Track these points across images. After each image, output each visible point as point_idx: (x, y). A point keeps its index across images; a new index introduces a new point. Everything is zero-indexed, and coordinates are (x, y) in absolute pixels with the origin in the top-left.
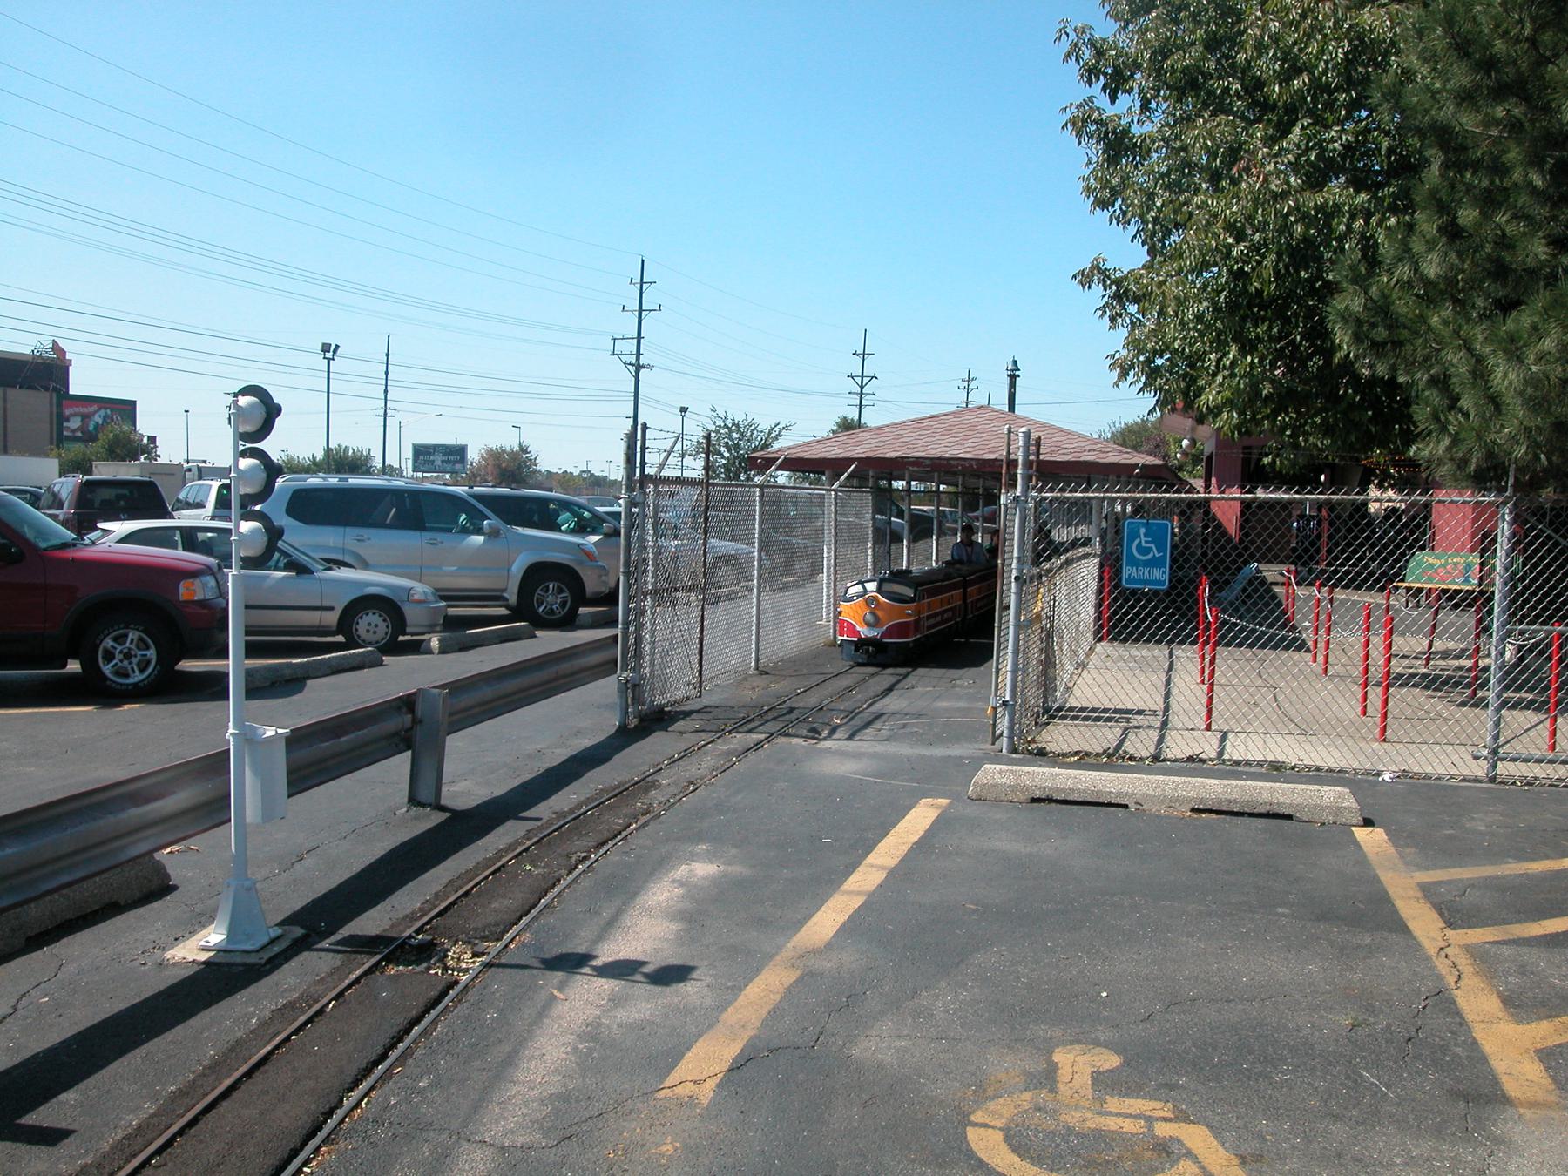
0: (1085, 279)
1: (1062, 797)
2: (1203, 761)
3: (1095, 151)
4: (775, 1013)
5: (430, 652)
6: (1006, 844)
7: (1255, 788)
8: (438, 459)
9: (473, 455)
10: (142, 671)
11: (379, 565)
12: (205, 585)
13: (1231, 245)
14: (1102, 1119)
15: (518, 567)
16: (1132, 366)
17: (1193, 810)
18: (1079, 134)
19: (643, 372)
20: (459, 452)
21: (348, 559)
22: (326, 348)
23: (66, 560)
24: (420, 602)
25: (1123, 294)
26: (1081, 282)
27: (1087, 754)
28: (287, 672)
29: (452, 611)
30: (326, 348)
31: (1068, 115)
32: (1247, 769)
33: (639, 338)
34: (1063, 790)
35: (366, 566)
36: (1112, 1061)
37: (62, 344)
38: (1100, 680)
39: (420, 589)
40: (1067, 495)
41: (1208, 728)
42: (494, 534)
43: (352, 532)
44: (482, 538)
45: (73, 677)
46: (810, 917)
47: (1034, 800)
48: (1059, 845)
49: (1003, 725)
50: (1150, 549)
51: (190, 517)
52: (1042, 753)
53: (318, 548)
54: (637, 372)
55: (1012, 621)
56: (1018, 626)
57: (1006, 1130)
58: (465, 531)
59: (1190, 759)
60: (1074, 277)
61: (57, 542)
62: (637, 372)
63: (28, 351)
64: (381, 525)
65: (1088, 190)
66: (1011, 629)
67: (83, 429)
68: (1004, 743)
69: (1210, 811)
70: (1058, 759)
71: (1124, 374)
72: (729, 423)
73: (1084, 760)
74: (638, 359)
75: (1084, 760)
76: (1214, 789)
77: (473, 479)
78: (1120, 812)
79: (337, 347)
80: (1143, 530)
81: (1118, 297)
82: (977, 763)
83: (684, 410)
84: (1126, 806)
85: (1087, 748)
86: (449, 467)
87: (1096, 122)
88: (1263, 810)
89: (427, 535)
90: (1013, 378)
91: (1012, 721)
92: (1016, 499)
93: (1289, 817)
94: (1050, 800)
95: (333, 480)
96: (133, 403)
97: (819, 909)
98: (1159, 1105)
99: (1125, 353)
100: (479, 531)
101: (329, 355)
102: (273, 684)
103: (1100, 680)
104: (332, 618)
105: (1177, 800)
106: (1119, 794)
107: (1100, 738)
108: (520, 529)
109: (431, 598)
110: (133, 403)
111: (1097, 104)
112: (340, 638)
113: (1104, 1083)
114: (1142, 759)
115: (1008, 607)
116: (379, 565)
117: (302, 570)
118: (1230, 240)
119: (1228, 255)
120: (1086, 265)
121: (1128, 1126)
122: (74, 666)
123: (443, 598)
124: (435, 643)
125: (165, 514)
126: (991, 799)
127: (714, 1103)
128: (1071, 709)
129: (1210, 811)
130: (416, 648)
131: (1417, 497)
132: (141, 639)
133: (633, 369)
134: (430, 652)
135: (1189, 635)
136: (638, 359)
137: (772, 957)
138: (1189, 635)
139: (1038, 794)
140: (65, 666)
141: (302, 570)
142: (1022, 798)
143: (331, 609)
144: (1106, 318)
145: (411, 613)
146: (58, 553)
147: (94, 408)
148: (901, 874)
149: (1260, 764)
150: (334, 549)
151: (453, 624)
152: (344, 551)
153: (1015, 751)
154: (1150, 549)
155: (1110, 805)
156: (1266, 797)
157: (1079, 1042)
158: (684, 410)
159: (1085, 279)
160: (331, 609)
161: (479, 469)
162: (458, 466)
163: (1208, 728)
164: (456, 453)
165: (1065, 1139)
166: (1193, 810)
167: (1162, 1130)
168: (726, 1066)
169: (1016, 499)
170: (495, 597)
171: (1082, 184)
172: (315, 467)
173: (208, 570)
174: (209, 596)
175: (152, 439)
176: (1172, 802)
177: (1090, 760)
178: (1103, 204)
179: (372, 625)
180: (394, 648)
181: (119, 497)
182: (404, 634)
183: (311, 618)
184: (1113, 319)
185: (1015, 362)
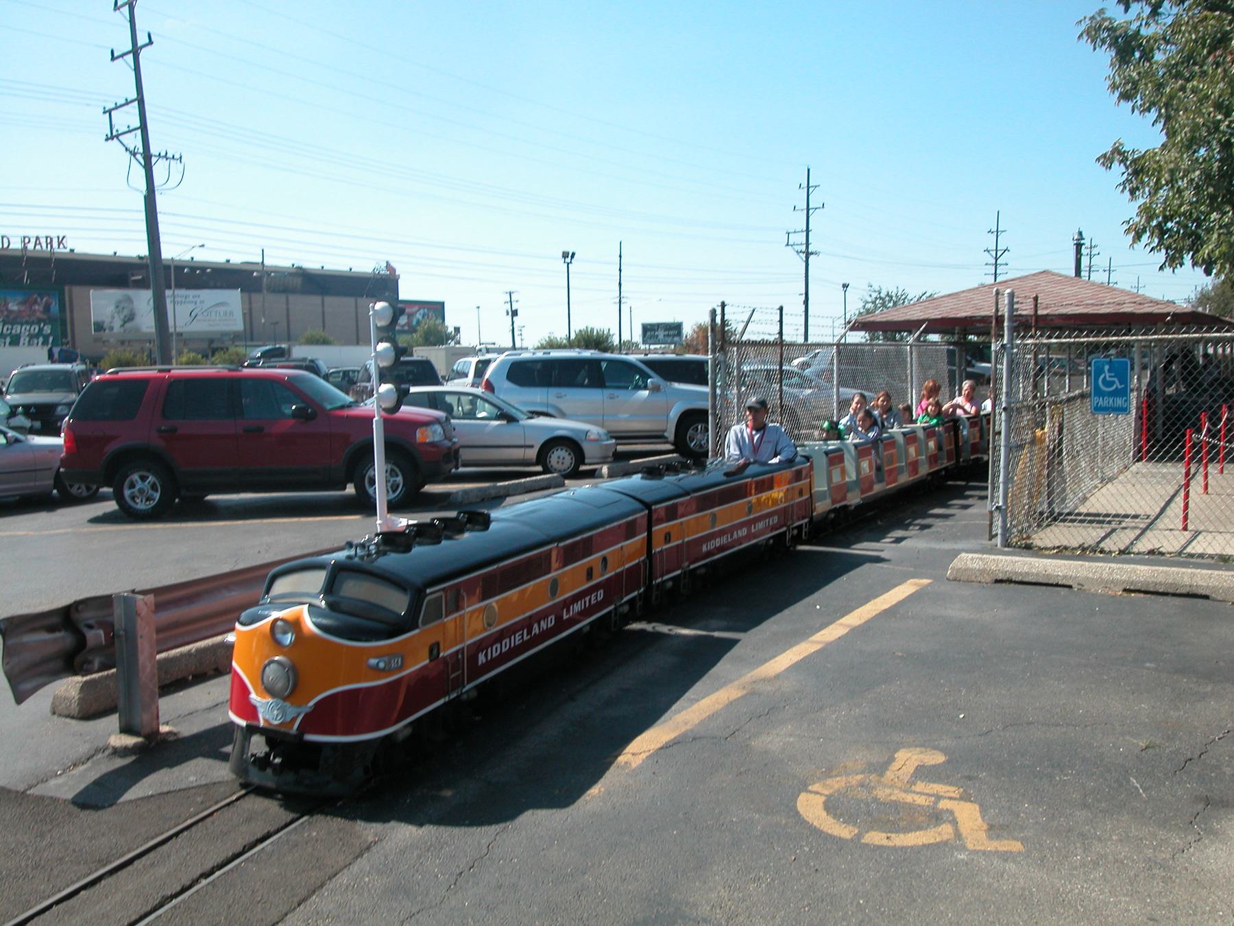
0: (1106, 160)
1: (1020, 578)
2: (1162, 554)
3: (1106, 56)
4: (711, 717)
5: (601, 476)
6: (955, 612)
7: (1178, 573)
8: (661, 334)
9: (688, 330)
10: (394, 491)
11: (576, 415)
12: (435, 432)
13: (1220, 121)
14: (904, 795)
15: (674, 414)
16: (1144, 231)
17: (1125, 590)
18: (1094, 41)
19: (811, 258)
20: (676, 328)
21: (551, 411)
22: (565, 255)
23: (342, 417)
24: (597, 440)
25: (1139, 171)
26: (1103, 164)
27: (1066, 548)
28: (493, 493)
29: (620, 448)
30: (565, 255)
31: (1083, 27)
32: (1199, 560)
33: (808, 231)
34: (1021, 574)
35: (563, 415)
36: (939, 758)
37: (393, 264)
38: (1123, 490)
39: (595, 430)
40: (1053, 341)
41: (1185, 529)
42: (656, 389)
43: (553, 391)
44: (646, 393)
45: (349, 498)
46: (775, 657)
47: (997, 581)
48: (1003, 615)
49: (998, 523)
50: (1114, 382)
51: (458, 385)
52: (1028, 547)
53: (525, 403)
54: (807, 258)
55: (1003, 443)
56: (1009, 449)
57: (829, 797)
58: (637, 388)
59: (1151, 552)
60: (1098, 159)
61: (339, 404)
62: (807, 258)
63: (370, 271)
64: (582, 386)
65: (1114, 87)
66: (1002, 449)
67: (409, 324)
68: (999, 540)
69: (1139, 591)
70: (1039, 552)
71: (1138, 237)
72: (883, 295)
73: (1062, 552)
74: (807, 247)
75: (1062, 552)
76: (1143, 573)
77: (690, 347)
78: (1063, 591)
79: (573, 254)
80: (1107, 367)
81: (1136, 173)
82: (956, 553)
83: (845, 286)
84: (1070, 587)
85: (1065, 543)
86: (669, 340)
87: (1108, 29)
88: (1184, 591)
89: (607, 392)
90: (1079, 246)
91: (1004, 522)
92: (1003, 346)
93: (1206, 597)
94: (1010, 581)
95: (587, 354)
96: (442, 304)
97: (784, 651)
98: (954, 789)
99: (1137, 219)
100: (645, 388)
101: (568, 260)
102: (483, 500)
103: (1123, 490)
104: (532, 454)
105: (1112, 581)
106: (1065, 577)
107: (1091, 534)
108: (676, 385)
109: (604, 437)
110: (442, 304)
111: (1108, 15)
112: (539, 468)
113: (924, 773)
114: (1110, 552)
115: (1000, 433)
116: (576, 415)
117: (511, 419)
118: (1219, 117)
119: (1217, 129)
120: (1108, 149)
121: (921, 800)
122: (350, 489)
123: (612, 437)
124: (605, 470)
125: (437, 383)
126: (964, 579)
127: (640, 767)
128: (1079, 514)
129: (1139, 591)
130: (591, 474)
131: (982, 339)
132: (392, 470)
133: (803, 256)
134: (601, 476)
135: (1178, 452)
136: (807, 247)
137: (731, 681)
138: (1178, 452)
139: (1000, 576)
140: (344, 488)
141: (511, 419)
142: (989, 580)
143: (532, 447)
144: (1127, 193)
145: (588, 449)
146: (346, 412)
147: (415, 309)
148: (856, 632)
149: (1211, 556)
150: (541, 404)
151: (619, 457)
152: (547, 405)
153: (1009, 546)
154: (1114, 382)
155: (1057, 585)
156: (1187, 581)
157: (921, 746)
158: (845, 286)
159: (1106, 160)
160: (532, 447)
161: (692, 339)
162: (676, 339)
163: (1185, 529)
164: (674, 329)
165: (867, 805)
166: (1125, 590)
167: (943, 805)
168: (659, 745)
169: (1003, 346)
170: (658, 437)
171: (1109, 83)
172: (570, 345)
173: (437, 421)
174: (437, 439)
175: (457, 330)
176: (1106, 584)
177: (1067, 553)
178: (1126, 96)
179: (561, 458)
180: (576, 474)
181: (408, 373)
182: (584, 464)
183: (518, 454)
184: (1132, 192)
185: (1080, 233)
